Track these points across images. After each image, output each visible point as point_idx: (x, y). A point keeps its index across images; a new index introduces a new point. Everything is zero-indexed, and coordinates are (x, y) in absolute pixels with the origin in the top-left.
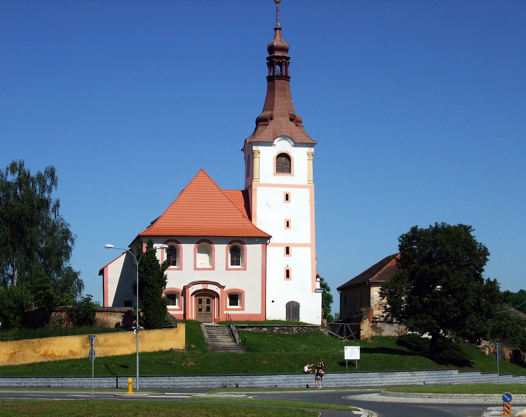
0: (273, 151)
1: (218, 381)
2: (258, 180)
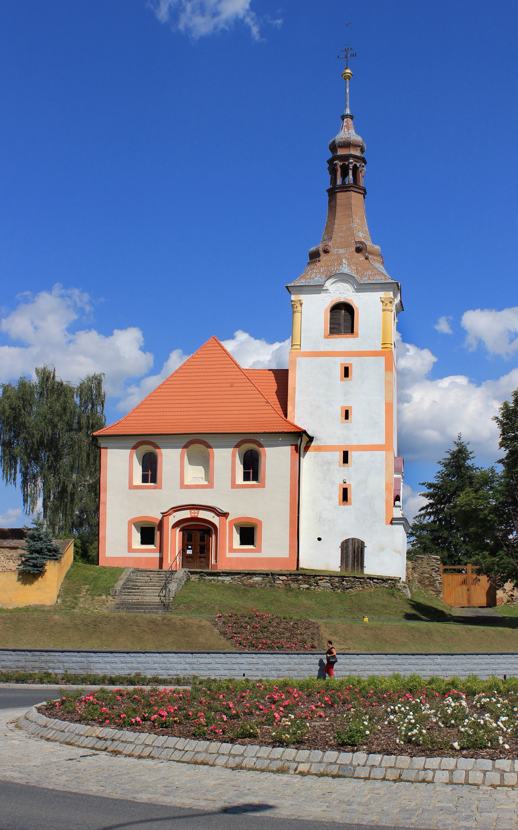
0: (323, 300)
1: (17, 660)
2: (298, 347)
